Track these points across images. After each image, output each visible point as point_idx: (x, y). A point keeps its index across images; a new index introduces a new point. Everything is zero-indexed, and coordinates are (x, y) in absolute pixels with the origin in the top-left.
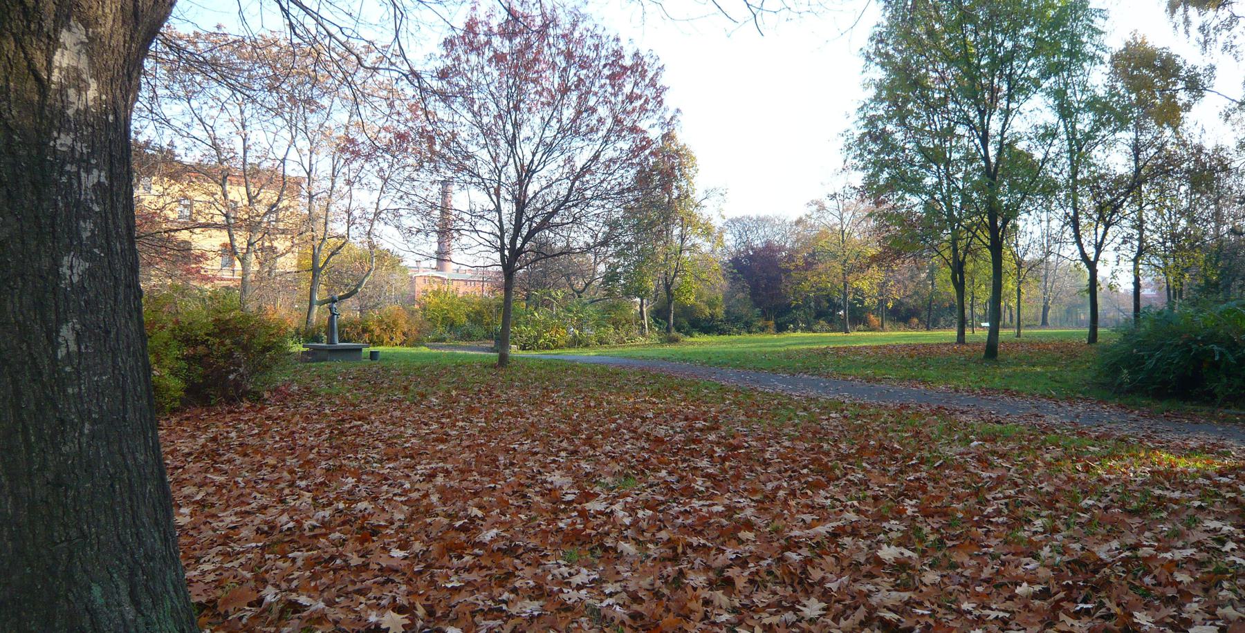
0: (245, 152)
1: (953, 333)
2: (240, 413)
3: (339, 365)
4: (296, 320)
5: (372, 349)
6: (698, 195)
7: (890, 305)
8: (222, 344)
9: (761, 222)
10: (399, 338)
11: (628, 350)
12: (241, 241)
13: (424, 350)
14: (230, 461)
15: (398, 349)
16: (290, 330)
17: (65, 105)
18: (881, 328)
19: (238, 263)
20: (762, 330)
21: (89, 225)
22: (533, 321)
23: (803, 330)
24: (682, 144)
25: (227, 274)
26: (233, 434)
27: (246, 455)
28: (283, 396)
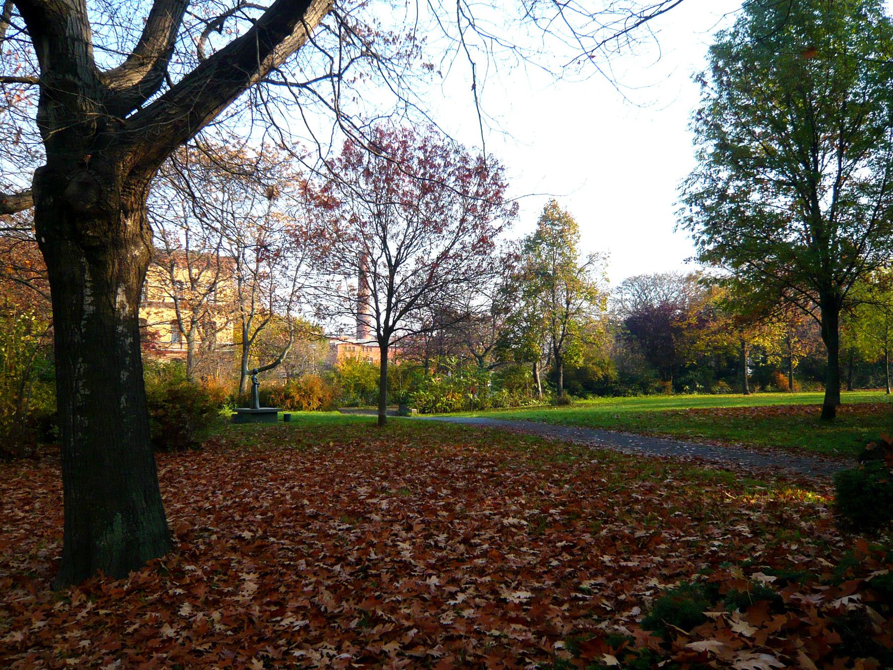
0: (187, 243)
1: (846, 395)
2: (187, 456)
3: (258, 426)
4: (231, 388)
5: (287, 413)
6: (580, 262)
7: (795, 363)
8: (174, 407)
9: (657, 281)
10: (315, 404)
11: (518, 412)
12: (186, 314)
13: (336, 413)
14: (180, 482)
15: (315, 413)
16: (227, 397)
17: (120, 315)
18: (791, 388)
19: (184, 338)
20: (660, 391)
21: (128, 359)
22: (432, 386)
23: (700, 391)
24: (564, 212)
25: (176, 347)
26: (182, 469)
27: (189, 479)
28: (215, 446)
